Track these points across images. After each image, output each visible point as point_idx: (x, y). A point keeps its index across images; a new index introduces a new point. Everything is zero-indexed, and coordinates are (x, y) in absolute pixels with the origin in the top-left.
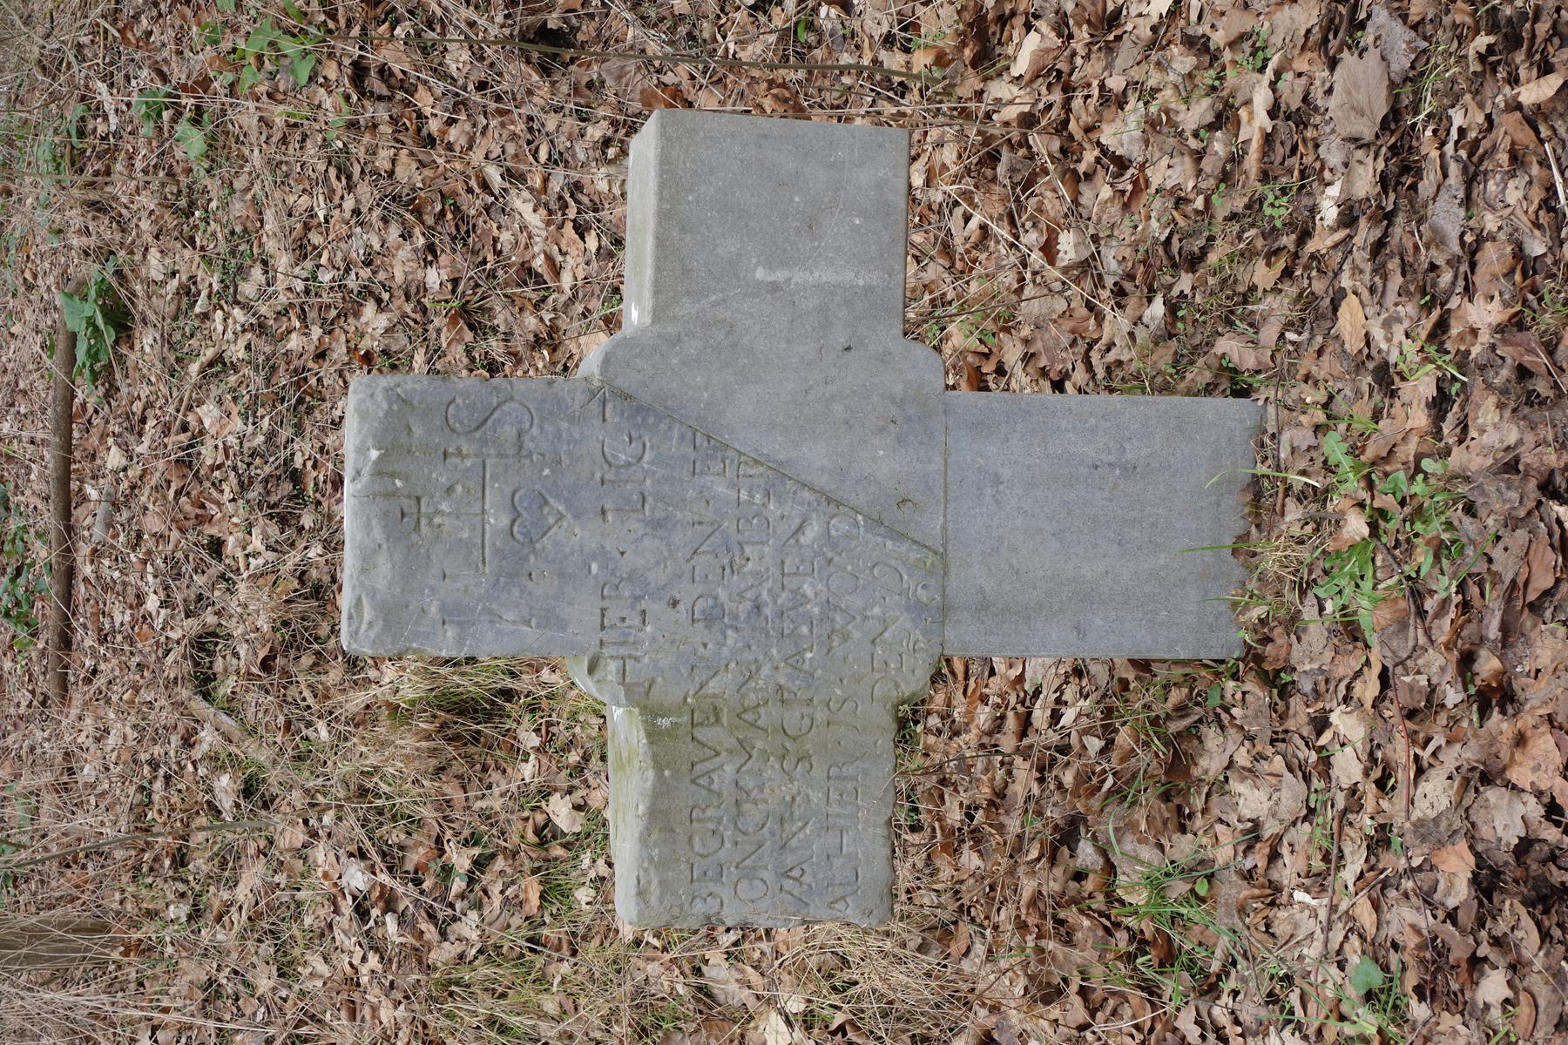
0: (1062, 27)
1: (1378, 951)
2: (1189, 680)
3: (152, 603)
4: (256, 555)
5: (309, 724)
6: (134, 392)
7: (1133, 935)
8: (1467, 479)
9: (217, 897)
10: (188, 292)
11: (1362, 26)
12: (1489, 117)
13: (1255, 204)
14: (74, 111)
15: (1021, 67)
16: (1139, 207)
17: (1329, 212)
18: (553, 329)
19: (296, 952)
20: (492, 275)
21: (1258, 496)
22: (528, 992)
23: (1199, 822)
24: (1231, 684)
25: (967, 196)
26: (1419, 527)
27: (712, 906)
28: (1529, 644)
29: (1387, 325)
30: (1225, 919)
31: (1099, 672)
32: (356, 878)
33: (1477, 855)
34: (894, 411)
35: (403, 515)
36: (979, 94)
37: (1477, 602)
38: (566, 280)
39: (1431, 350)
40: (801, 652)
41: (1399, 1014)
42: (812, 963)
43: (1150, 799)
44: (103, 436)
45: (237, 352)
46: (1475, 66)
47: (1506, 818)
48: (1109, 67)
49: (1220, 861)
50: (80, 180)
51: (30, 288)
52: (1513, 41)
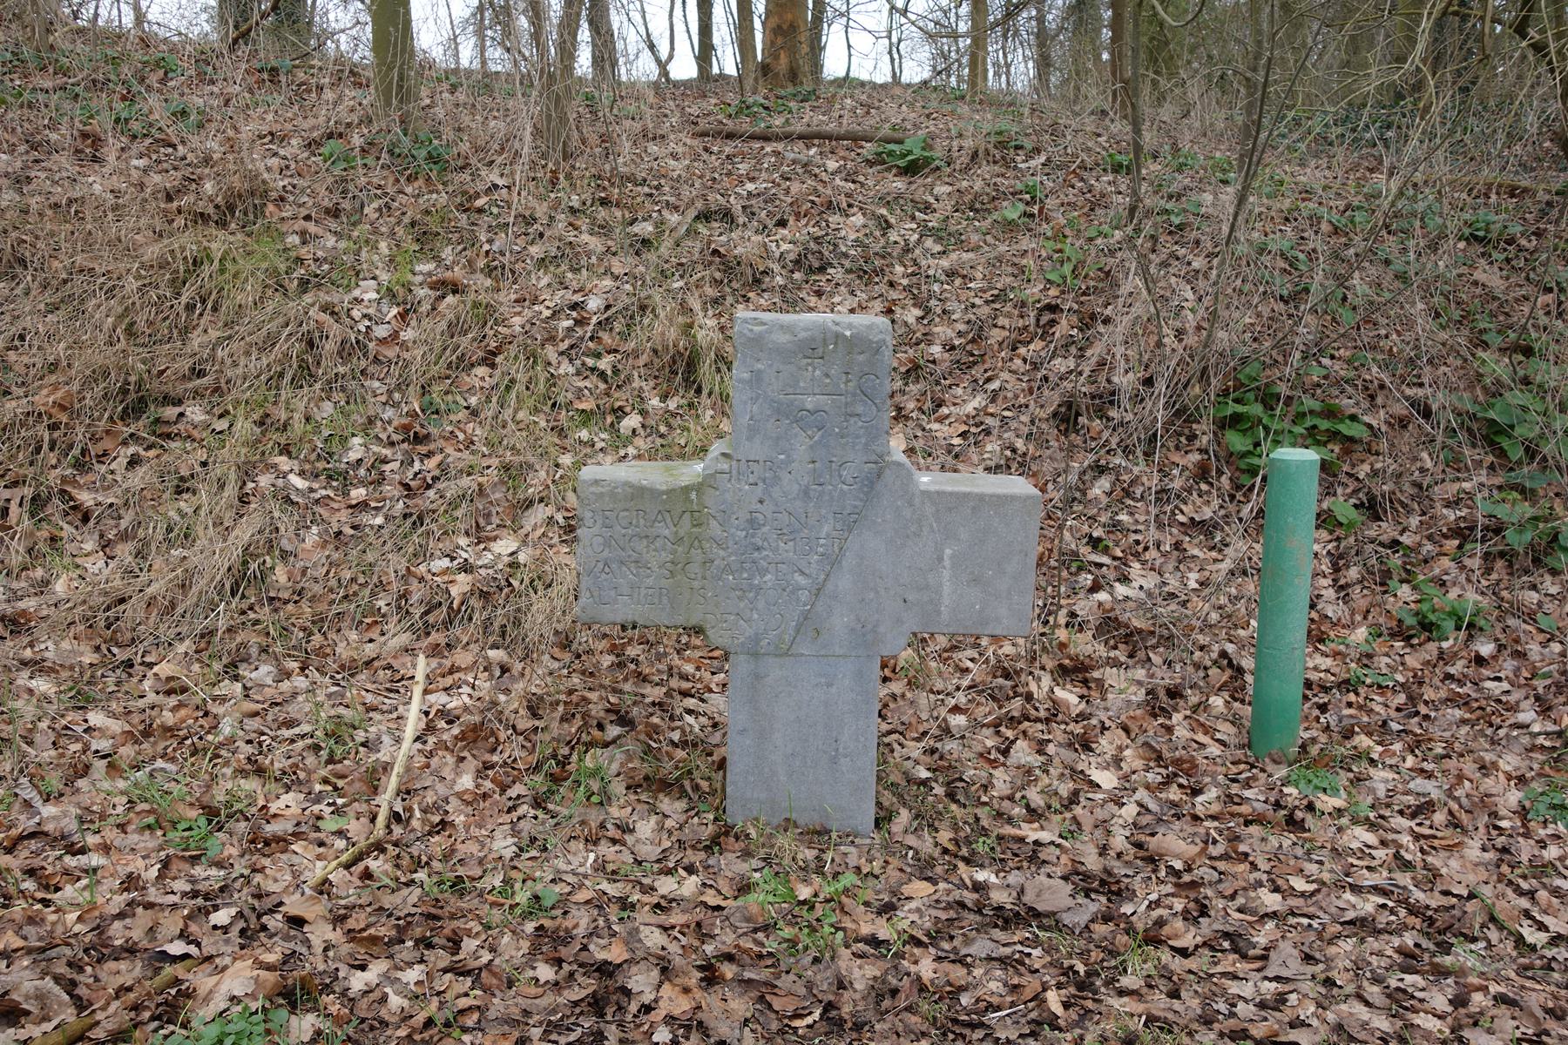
0: (1082, 717)
1: (563, 903)
2: (713, 792)
3: (750, 186)
4: (778, 246)
5: (682, 277)
6: (870, 176)
7: (567, 757)
8: (833, 958)
9: (583, 223)
10: (927, 208)
11: (1087, 896)
12: (1037, 971)
13: (985, 832)
14: (1028, 145)
15: (1060, 693)
16: (982, 763)
17: (981, 876)
18: (907, 418)
19: (552, 268)
20: (938, 383)
21: (819, 833)
22: (531, 402)
23: (633, 797)
24: (711, 817)
25: (987, 661)
26: (806, 931)
27: (589, 522)
28: (741, 995)
29: (918, 910)
30: (577, 811)
31: (716, 738)
32: (594, 303)
33: (620, 965)
34: (869, 627)
35: (814, 348)
36: (1043, 668)
37: (763, 963)
38: (935, 426)
39: (906, 937)
40: (732, 573)
41: (527, 915)
42: (547, 567)
43: (646, 769)
44: (844, 158)
45: (893, 236)
46: (1066, 963)
47: (641, 982)
48: (1060, 745)
49: (611, 810)
50: (990, 147)
51: (928, 116)
52: (1081, 986)
